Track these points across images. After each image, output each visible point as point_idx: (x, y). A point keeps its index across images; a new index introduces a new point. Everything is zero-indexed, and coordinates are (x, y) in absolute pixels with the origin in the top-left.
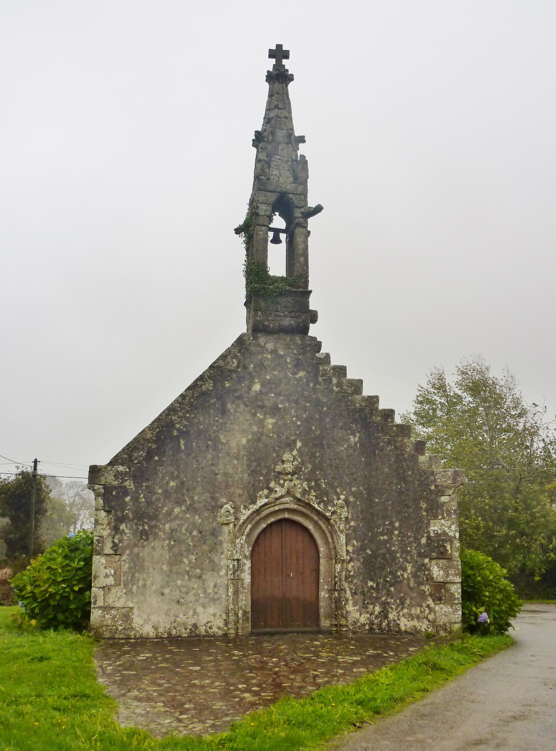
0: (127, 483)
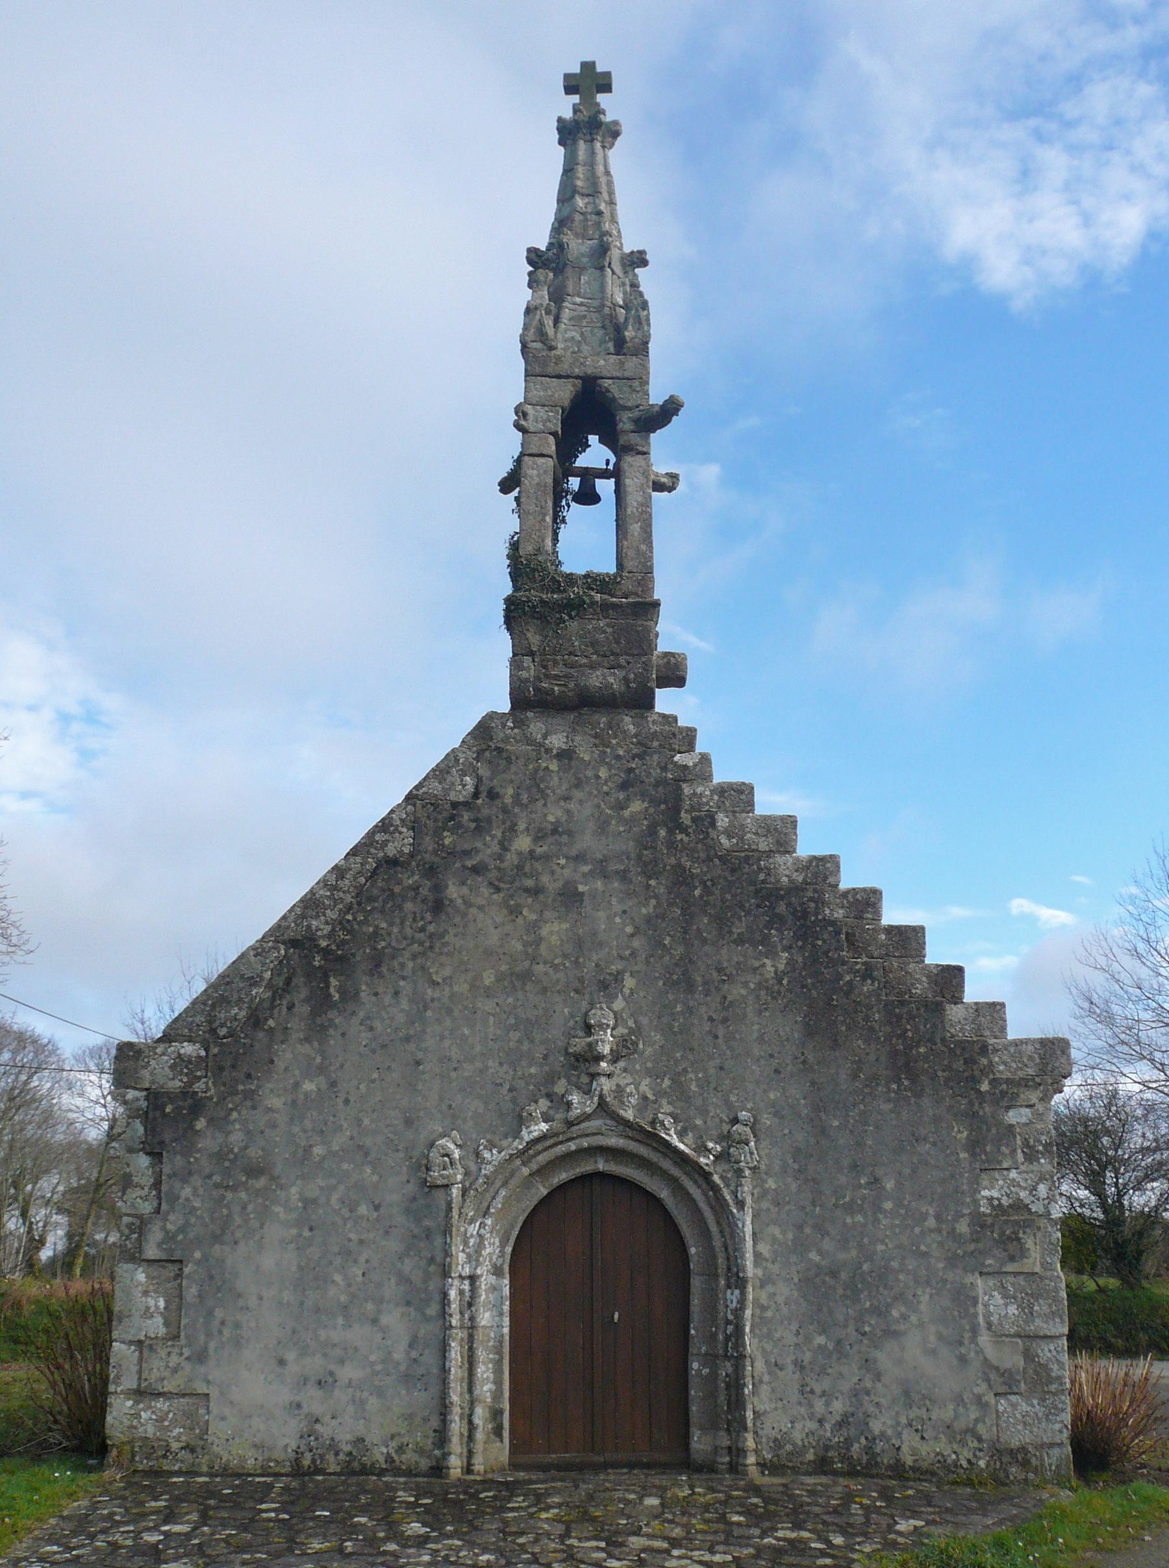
0: (199, 1086)
